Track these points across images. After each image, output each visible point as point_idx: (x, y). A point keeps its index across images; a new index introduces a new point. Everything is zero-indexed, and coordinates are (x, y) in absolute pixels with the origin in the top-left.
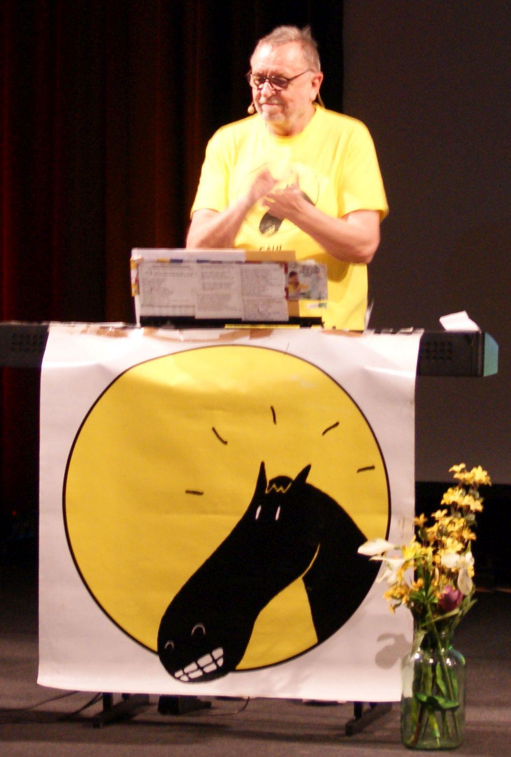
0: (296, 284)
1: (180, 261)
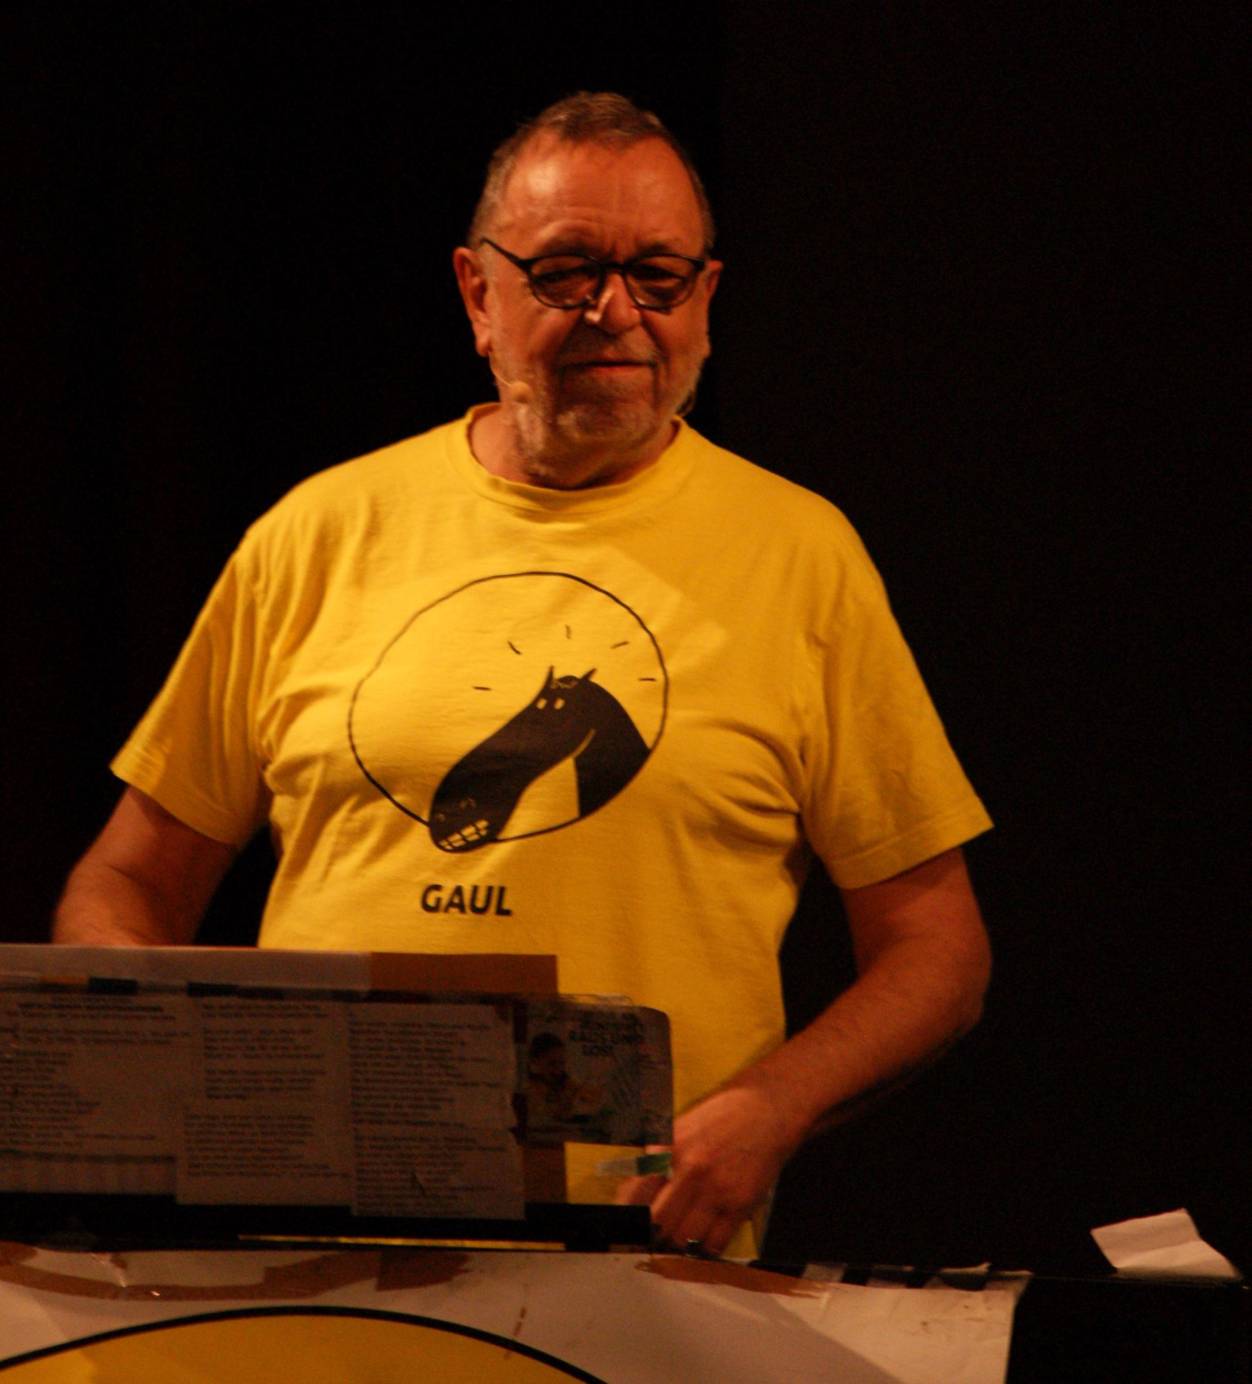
0: (558, 1082)
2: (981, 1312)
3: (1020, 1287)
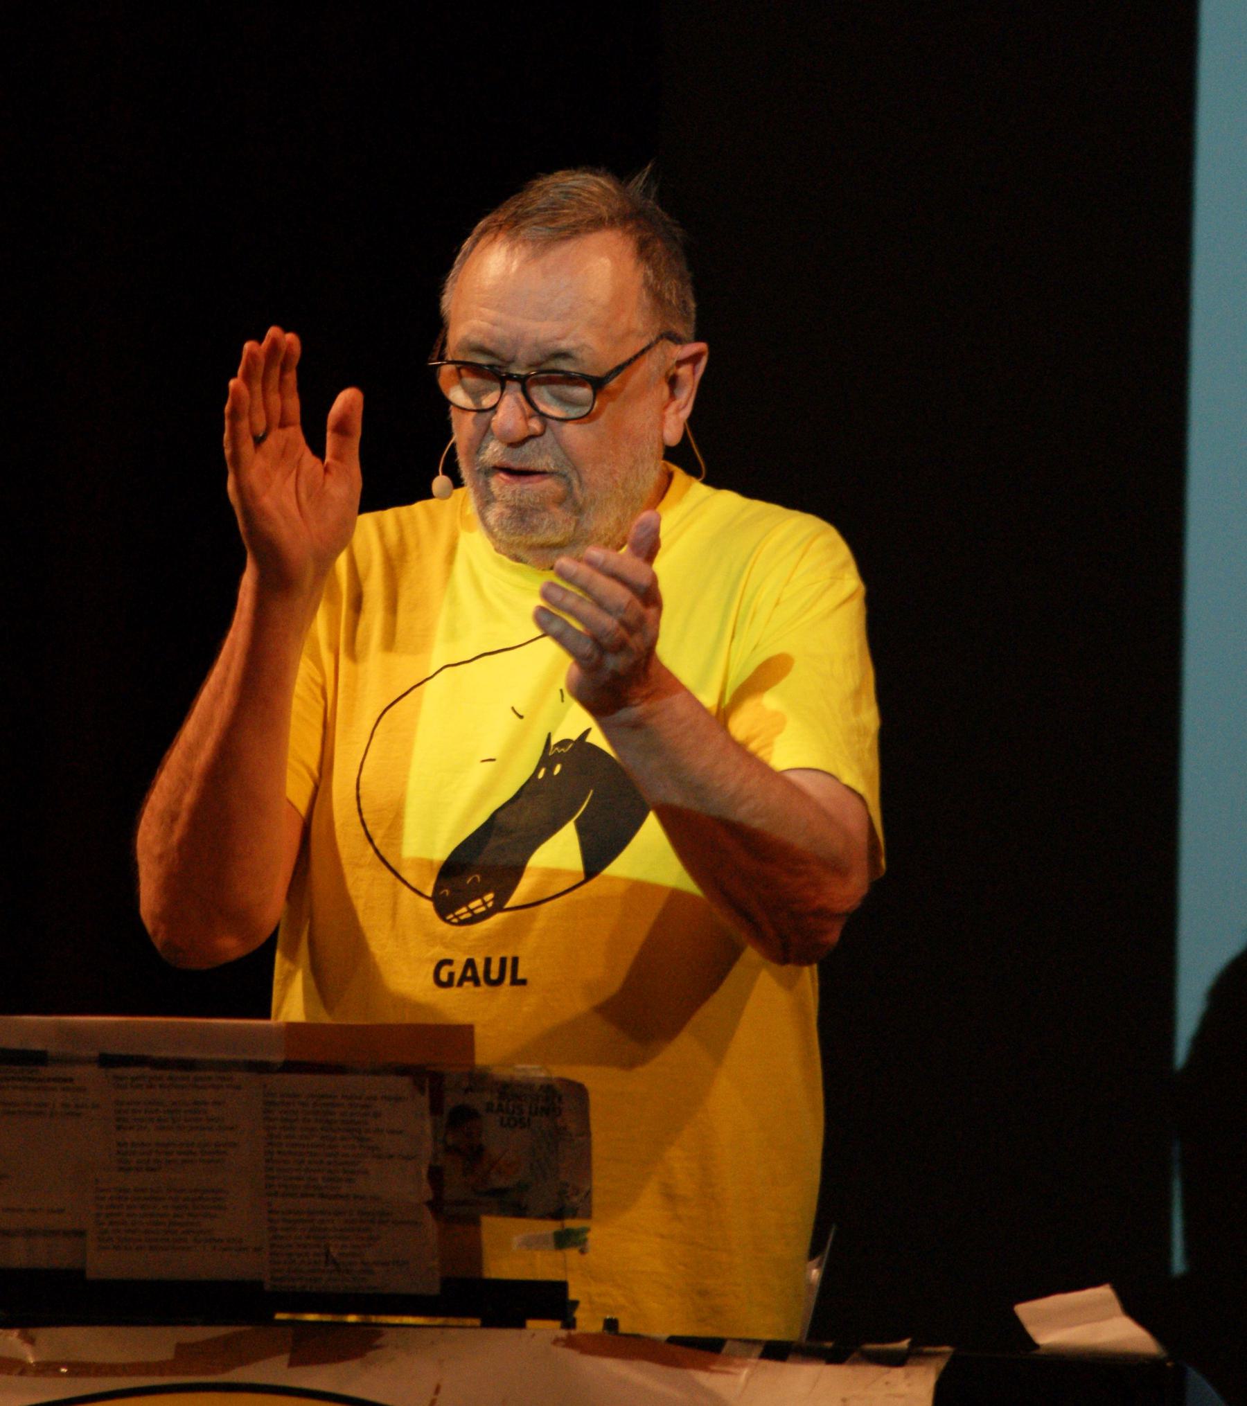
0: (473, 1154)
1: (38, 1058)
2: (902, 1388)
3: (941, 1363)
